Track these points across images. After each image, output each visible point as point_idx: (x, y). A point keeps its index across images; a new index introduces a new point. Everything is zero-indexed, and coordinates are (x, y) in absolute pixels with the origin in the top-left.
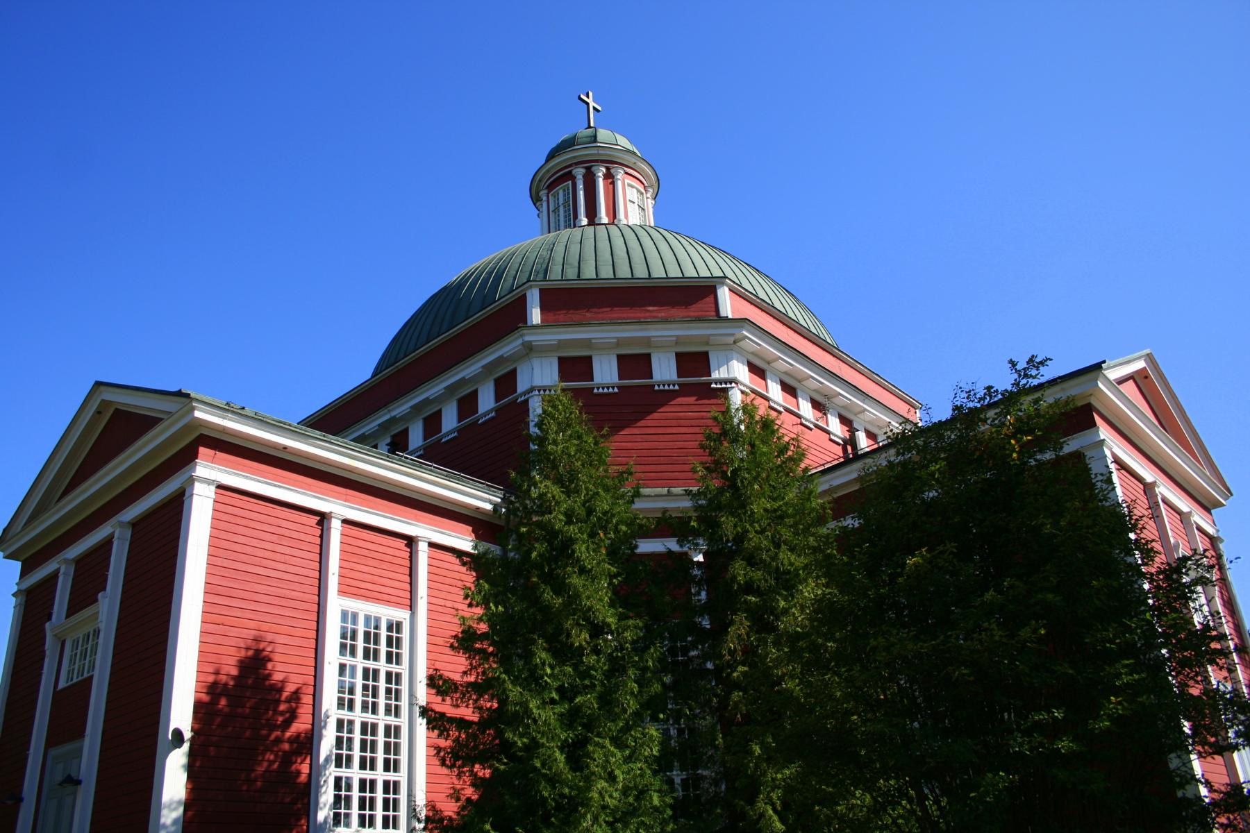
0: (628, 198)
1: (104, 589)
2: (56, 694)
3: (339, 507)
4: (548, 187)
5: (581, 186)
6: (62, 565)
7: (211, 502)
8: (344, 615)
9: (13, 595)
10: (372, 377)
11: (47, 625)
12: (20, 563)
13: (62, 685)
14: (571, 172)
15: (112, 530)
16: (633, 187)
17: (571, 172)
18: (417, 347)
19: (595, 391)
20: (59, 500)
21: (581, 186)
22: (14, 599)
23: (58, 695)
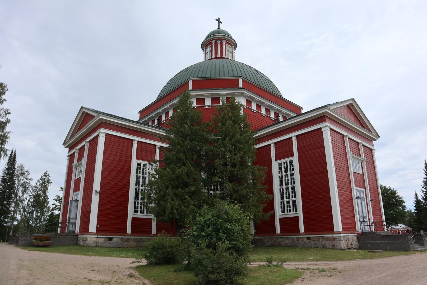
0: (227, 49)
1: (83, 157)
2: (75, 180)
3: (136, 139)
4: (206, 46)
5: (213, 46)
6: (76, 150)
7: (105, 137)
8: (138, 164)
9: (67, 156)
10: (156, 100)
11: (73, 165)
12: (68, 149)
13: (76, 179)
14: (211, 42)
15: (85, 143)
16: (228, 46)
17: (211, 42)
18: (178, 85)
19: (205, 107)
20: (76, 134)
21: (213, 46)
22: (67, 157)
23: (75, 180)
